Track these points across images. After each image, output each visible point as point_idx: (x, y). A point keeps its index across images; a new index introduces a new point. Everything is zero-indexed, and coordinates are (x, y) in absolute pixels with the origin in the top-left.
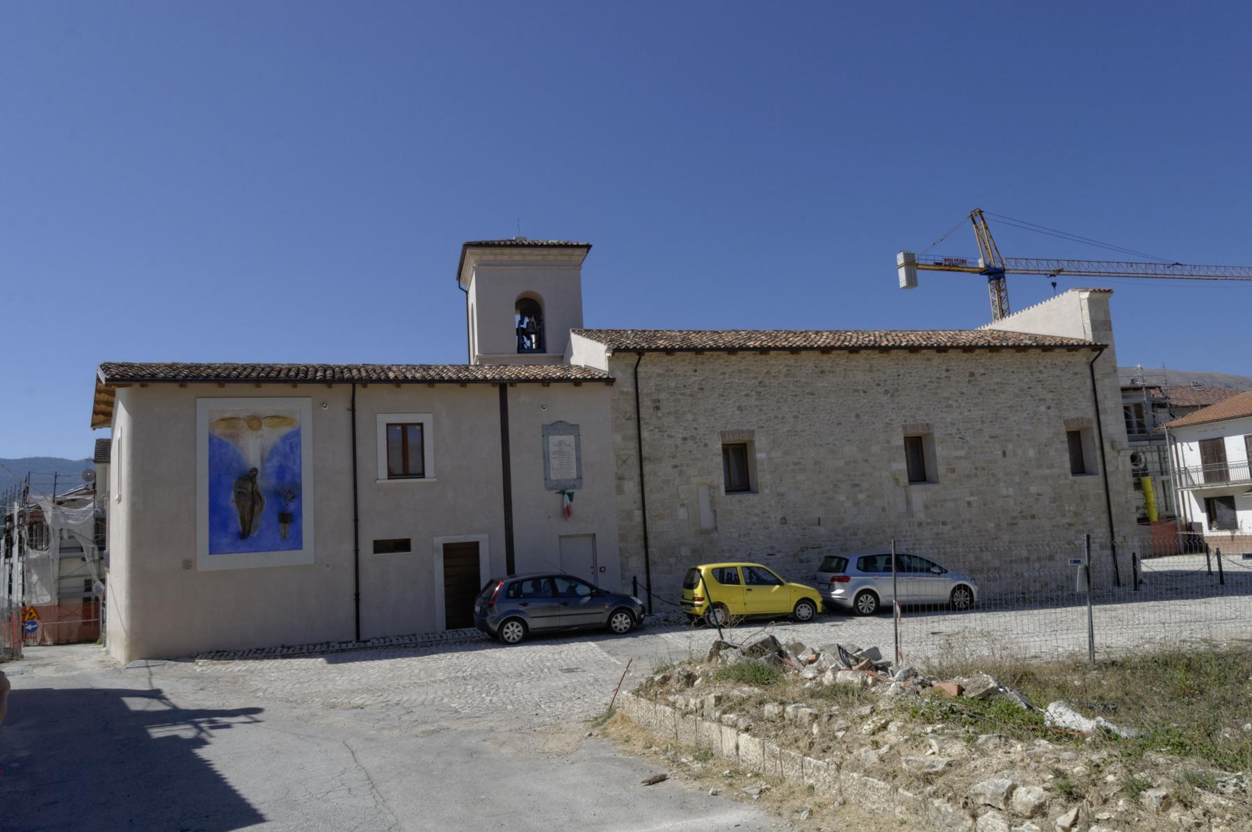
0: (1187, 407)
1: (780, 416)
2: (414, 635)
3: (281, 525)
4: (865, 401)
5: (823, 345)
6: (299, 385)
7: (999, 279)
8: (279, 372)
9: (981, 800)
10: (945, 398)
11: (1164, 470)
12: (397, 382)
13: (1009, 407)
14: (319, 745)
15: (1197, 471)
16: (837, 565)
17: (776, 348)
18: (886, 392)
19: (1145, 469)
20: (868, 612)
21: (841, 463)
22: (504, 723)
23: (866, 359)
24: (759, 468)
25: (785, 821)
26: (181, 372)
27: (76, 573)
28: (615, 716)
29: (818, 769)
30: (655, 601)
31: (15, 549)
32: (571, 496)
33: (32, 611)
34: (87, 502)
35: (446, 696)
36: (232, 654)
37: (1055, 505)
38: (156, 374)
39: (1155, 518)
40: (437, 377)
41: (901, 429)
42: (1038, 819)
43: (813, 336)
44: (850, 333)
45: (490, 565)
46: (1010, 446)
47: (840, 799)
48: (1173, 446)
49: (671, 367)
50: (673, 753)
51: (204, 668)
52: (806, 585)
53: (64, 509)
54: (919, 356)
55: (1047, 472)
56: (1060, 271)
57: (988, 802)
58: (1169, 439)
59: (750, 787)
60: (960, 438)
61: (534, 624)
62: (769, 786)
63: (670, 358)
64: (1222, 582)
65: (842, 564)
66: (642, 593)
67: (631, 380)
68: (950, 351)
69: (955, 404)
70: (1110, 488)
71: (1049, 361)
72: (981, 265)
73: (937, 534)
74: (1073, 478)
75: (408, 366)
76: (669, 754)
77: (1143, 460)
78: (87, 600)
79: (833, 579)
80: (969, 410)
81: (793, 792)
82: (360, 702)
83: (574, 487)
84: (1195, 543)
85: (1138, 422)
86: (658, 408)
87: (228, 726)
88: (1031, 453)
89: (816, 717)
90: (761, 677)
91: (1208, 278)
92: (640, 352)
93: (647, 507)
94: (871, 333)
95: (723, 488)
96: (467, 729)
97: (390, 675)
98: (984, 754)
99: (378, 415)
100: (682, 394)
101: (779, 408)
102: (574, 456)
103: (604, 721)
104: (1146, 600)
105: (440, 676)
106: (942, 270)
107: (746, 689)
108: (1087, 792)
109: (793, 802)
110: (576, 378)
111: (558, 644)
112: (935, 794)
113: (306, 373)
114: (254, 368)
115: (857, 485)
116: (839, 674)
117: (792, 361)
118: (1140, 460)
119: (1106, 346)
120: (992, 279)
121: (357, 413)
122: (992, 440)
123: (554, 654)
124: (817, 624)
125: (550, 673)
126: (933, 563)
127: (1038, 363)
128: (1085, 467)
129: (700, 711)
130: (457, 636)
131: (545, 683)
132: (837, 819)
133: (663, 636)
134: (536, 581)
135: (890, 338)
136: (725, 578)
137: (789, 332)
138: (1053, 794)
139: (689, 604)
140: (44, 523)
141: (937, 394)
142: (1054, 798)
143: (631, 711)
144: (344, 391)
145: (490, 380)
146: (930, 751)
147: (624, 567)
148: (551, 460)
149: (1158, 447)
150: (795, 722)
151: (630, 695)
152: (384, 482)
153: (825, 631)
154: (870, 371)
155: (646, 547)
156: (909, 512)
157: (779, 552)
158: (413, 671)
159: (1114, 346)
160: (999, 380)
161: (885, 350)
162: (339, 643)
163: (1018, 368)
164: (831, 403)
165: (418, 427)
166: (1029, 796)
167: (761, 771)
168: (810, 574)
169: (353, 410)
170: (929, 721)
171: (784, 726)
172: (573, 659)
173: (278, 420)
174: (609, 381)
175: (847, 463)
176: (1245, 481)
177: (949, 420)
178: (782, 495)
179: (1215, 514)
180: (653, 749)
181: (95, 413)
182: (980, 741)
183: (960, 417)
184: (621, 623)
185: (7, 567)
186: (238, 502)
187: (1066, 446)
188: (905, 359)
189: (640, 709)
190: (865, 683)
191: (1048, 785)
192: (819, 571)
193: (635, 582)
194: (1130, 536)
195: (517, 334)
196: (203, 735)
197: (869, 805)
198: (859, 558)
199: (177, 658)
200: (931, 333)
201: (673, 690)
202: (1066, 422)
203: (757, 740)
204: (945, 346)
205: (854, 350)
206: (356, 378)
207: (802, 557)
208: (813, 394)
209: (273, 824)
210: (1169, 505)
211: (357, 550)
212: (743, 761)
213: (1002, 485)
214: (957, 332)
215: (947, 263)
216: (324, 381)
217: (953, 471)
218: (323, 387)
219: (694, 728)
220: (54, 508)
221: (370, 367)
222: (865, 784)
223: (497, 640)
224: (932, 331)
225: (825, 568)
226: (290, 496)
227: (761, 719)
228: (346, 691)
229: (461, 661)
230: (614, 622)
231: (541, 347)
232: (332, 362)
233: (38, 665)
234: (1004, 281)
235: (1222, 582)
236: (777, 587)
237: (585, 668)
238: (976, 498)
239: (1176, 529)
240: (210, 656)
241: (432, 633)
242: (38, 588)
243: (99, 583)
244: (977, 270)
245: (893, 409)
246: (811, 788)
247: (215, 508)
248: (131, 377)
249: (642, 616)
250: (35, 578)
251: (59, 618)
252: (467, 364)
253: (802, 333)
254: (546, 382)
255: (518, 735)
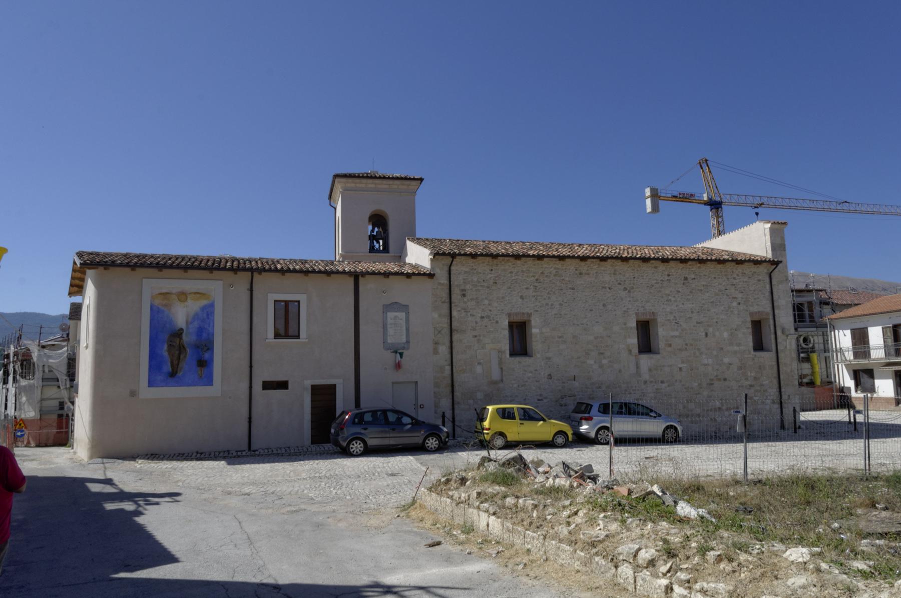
0: (845, 305)
1: (550, 304)
2: (289, 448)
3: (199, 368)
4: (610, 295)
5: (581, 255)
6: (214, 272)
7: (718, 208)
8: (201, 262)
9: (621, 558)
10: (666, 295)
11: (826, 349)
12: (283, 272)
13: (711, 302)
14: (217, 517)
15: (848, 351)
16: (585, 408)
17: (548, 256)
18: (625, 289)
19: (813, 348)
20: (605, 442)
21: (591, 338)
22: (343, 507)
23: (612, 266)
24: (533, 339)
25: (509, 570)
26: (132, 260)
27: (53, 397)
28: (416, 505)
29: (533, 538)
30: (458, 430)
31: (11, 378)
32: (401, 355)
33: (21, 422)
34: (63, 347)
35: (306, 488)
36: (162, 456)
37: (740, 372)
38: (115, 261)
39: (818, 382)
40: (310, 269)
41: (634, 315)
42: (651, 569)
43: (576, 248)
44: (603, 247)
45: (343, 401)
46: (711, 330)
47: (544, 557)
48: (833, 333)
49: (475, 267)
50: (449, 528)
51: (142, 465)
52: (560, 421)
53: (46, 351)
54: (649, 264)
55: (736, 348)
56: (762, 204)
57: (625, 558)
58: (830, 327)
59: (491, 549)
60: (676, 323)
61: (372, 442)
62: (504, 549)
63: (475, 260)
64: (855, 429)
65: (588, 408)
66: (449, 424)
67: (446, 275)
68: (671, 262)
69: (673, 299)
70: (780, 361)
71: (741, 271)
72: (706, 199)
73: (657, 389)
74: (755, 353)
75: (291, 260)
76: (446, 529)
77: (812, 341)
78: (60, 416)
79: (581, 419)
80: (683, 304)
81: (518, 553)
82: (247, 491)
83: (404, 348)
84: (844, 402)
85: (809, 315)
86: (464, 295)
87: (157, 504)
88: (726, 335)
89: (535, 506)
90: (505, 480)
91: (867, 212)
92: (453, 256)
93: (454, 364)
94: (618, 247)
95: (508, 352)
96: (317, 510)
97: (270, 474)
98: (628, 530)
99: (269, 294)
100: (481, 286)
101: (549, 298)
102: (405, 327)
103: (409, 507)
104: (799, 440)
105: (304, 475)
106: (677, 201)
107: (497, 488)
108: (680, 552)
109: (516, 559)
110: (408, 273)
111: (387, 457)
112: (597, 554)
113: (220, 263)
114: (183, 258)
115: (602, 354)
116: (557, 480)
117: (560, 265)
118: (810, 342)
119: (781, 262)
120: (712, 209)
121: (254, 292)
122: (698, 325)
123: (383, 463)
124: (568, 449)
125: (379, 476)
126: (650, 409)
127: (733, 272)
128: (764, 345)
129: (467, 502)
130: (318, 449)
131: (374, 482)
132: (540, 569)
133: (460, 453)
134: (374, 413)
135: (630, 251)
136: (506, 415)
137: (560, 244)
138: (661, 553)
139: (480, 432)
140: (32, 361)
141: (660, 291)
142: (660, 556)
143: (426, 502)
144: (245, 277)
145: (348, 272)
146: (598, 528)
147: (437, 406)
148: (389, 329)
149: (823, 332)
150: (523, 509)
151: (426, 490)
152: (271, 341)
153: (573, 454)
154: (614, 274)
155: (453, 392)
156: (638, 373)
157: (546, 398)
158: (286, 472)
159: (786, 262)
160: (705, 283)
161: (626, 260)
162: (237, 451)
163: (719, 275)
164: (585, 296)
165: (296, 304)
166: (647, 555)
167: (501, 540)
168: (567, 414)
169: (251, 290)
170: (605, 510)
171: (517, 512)
172: (396, 467)
173: (198, 295)
174: (431, 276)
175: (596, 338)
176: (881, 359)
177: (668, 310)
178: (549, 358)
179: (860, 381)
180: (437, 526)
181: (72, 285)
182: (628, 522)
183: (676, 308)
184: (432, 444)
185: (4, 391)
186: (169, 351)
187: (750, 330)
188: (639, 266)
189: (431, 500)
190: (571, 486)
191: (658, 548)
192: (572, 412)
193: (443, 416)
194: (793, 394)
195: (370, 239)
196: (140, 509)
197: (561, 561)
198: (600, 404)
199: (124, 458)
200: (660, 248)
201: (452, 488)
202: (751, 314)
203: (499, 520)
204: (668, 258)
205: (603, 259)
206: (254, 268)
207: (562, 403)
208: (573, 289)
209: (185, 563)
210: (829, 374)
211: (251, 388)
212: (491, 534)
213: (704, 356)
214: (679, 248)
215: (681, 196)
216: (232, 269)
217: (670, 345)
218: (230, 273)
219: (463, 512)
220: (39, 350)
221: (264, 260)
222: (559, 548)
223: (346, 453)
224: (661, 247)
225: (576, 411)
226: (205, 348)
227: (504, 507)
228: (238, 484)
229: (320, 466)
230: (427, 443)
231: (386, 249)
232: (239, 255)
233: (27, 460)
234: (721, 210)
235: (855, 429)
236: (542, 422)
237: (403, 474)
238: (685, 365)
239: (833, 391)
240: (147, 457)
241: (302, 447)
242: (26, 406)
243: (69, 404)
244: (702, 202)
245: (629, 301)
246: (529, 550)
247: (153, 355)
248: (98, 262)
249: (447, 440)
250: (24, 399)
251: (40, 428)
252: (334, 260)
253: (569, 245)
254: (387, 275)
255: (351, 515)
